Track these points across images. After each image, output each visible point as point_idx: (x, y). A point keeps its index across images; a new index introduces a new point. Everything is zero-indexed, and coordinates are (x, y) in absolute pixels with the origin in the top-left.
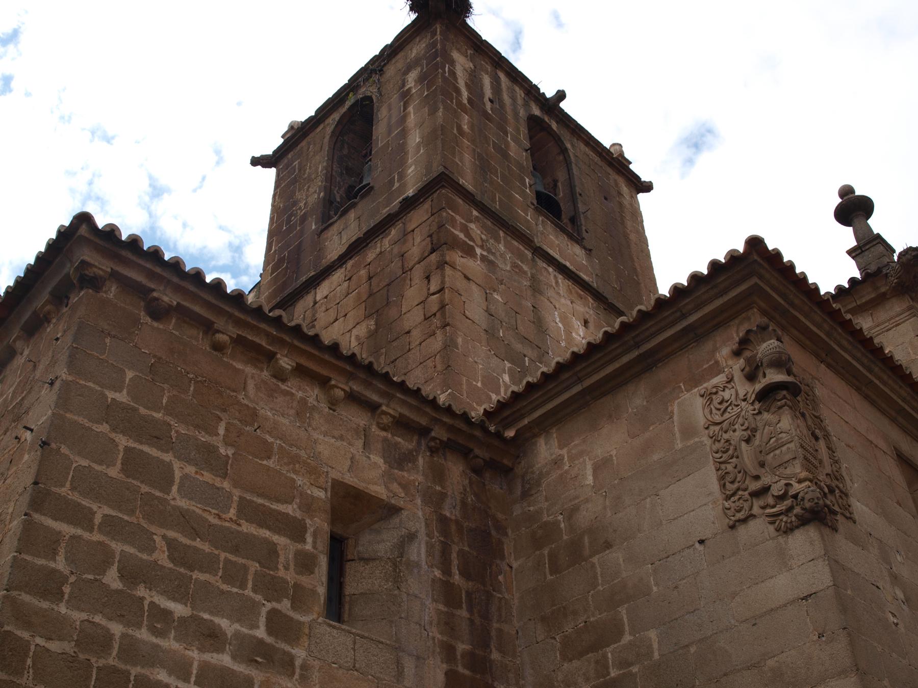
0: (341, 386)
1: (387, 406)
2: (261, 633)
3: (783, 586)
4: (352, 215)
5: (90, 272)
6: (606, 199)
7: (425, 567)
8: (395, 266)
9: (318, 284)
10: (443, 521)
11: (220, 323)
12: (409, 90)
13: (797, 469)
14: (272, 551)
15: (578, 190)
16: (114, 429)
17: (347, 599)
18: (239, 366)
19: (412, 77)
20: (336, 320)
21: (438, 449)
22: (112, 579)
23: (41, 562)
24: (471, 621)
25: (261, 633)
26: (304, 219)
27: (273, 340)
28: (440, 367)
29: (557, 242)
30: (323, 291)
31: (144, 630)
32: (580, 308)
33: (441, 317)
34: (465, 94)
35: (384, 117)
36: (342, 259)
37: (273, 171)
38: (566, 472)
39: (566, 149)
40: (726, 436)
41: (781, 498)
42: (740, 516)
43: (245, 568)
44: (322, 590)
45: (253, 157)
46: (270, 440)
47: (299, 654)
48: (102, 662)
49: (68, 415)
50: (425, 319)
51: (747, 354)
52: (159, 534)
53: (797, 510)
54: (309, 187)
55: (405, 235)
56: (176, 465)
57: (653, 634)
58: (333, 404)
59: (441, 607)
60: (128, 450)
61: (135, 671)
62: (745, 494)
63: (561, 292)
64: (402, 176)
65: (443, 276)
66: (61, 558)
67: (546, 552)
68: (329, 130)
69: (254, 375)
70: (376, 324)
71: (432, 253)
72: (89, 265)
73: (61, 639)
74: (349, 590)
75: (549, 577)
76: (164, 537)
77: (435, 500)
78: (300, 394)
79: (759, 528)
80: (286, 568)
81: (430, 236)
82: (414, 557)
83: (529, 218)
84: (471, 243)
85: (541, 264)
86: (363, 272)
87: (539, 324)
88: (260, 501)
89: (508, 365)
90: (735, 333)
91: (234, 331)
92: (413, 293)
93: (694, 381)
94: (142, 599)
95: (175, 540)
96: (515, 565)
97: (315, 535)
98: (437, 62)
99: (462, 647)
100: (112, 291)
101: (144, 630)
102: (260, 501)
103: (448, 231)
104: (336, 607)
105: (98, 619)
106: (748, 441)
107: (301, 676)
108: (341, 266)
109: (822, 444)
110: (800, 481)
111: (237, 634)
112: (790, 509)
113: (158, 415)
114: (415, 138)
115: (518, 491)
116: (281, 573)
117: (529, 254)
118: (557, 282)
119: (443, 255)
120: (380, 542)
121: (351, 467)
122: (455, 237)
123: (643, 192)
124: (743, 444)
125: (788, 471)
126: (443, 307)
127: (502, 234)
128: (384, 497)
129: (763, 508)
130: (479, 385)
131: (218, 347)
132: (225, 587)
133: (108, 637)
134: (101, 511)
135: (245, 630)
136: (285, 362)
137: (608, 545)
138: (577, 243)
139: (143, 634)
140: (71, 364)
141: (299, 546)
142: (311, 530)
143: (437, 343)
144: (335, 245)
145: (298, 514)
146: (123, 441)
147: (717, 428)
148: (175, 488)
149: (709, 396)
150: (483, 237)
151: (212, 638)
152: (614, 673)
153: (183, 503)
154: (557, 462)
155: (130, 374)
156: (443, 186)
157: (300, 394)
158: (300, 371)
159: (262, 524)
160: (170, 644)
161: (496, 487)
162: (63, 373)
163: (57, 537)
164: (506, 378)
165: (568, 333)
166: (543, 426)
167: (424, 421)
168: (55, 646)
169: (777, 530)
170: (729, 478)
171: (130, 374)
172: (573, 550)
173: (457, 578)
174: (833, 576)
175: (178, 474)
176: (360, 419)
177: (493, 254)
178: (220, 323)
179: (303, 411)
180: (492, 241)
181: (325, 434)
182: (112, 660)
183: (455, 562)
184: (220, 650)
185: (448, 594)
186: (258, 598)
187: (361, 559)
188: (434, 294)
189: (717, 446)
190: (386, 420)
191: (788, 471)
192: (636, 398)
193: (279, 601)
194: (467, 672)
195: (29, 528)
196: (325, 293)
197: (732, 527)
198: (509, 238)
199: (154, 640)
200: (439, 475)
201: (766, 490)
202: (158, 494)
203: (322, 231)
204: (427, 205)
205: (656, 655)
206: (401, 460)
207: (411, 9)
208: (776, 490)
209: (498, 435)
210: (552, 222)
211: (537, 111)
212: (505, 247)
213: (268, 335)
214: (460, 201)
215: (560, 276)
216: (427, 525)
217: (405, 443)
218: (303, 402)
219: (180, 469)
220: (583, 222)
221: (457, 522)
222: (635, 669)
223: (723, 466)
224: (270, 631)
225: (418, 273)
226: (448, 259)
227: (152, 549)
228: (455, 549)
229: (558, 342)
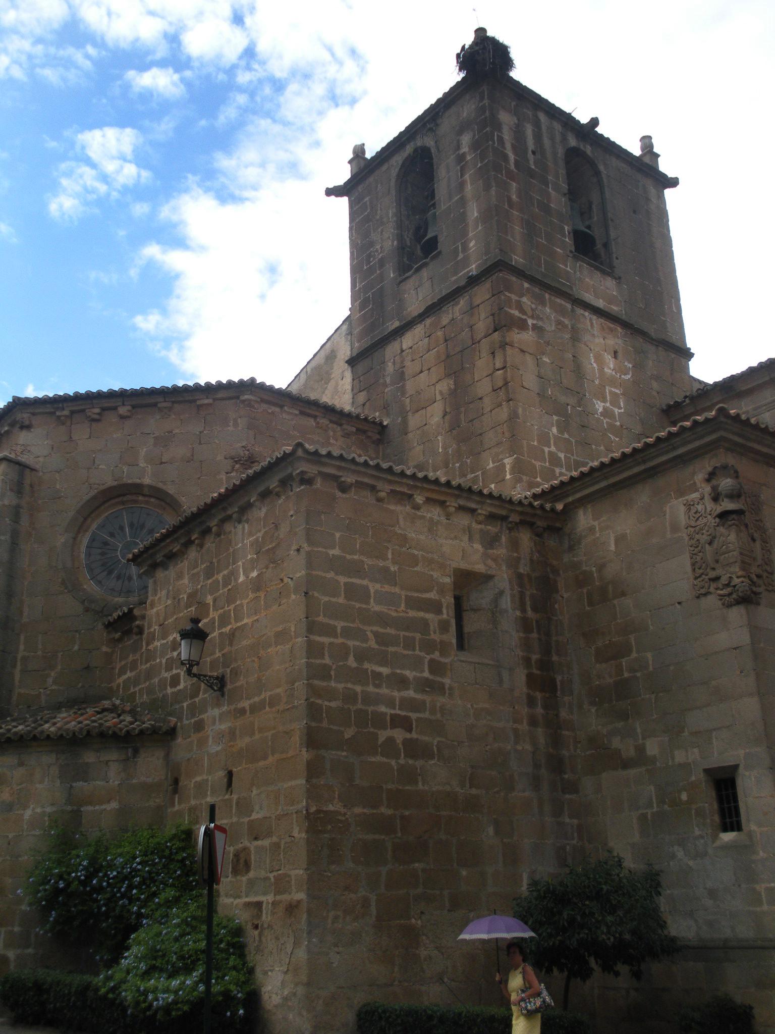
0: (453, 503)
1: (481, 509)
2: (426, 674)
3: (723, 639)
4: (425, 273)
5: (306, 477)
6: (634, 212)
7: (510, 611)
8: (466, 334)
9: (403, 334)
10: (520, 576)
11: (380, 485)
12: (464, 155)
13: (736, 569)
14: (425, 624)
15: (610, 215)
16: (336, 574)
17: (466, 635)
18: (392, 507)
19: (466, 140)
20: (421, 372)
21: (514, 527)
22: (352, 662)
23: (318, 661)
24: (540, 639)
25: (426, 674)
26: (382, 263)
27: (410, 487)
28: (507, 434)
29: (592, 283)
30: (407, 341)
31: (371, 686)
32: (611, 342)
33: (505, 390)
34: (512, 157)
35: (445, 174)
36: (422, 317)
37: (345, 200)
38: (598, 538)
39: (600, 172)
40: (697, 537)
41: (728, 585)
42: (703, 591)
43: (414, 638)
44: (454, 641)
45: (327, 189)
46: (416, 552)
47: (447, 681)
48: (355, 708)
49: (314, 573)
50: (494, 390)
51: (714, 482)
52: (369, 630)
53: (734, 596)
54: (382, 231)
55: (472, 308)
56: (371, 585)
57: (649, 655)
58: (448, 516)
59: (522, 635)
60: (345, 584)
61: (370, 709)
62: (706, 577)
63: (596, 333)
64: (465, 248)
65: (505, 356)
66: (327, 657)
67: (585, 591)
68: (394, 172)
69: (401, 510)
70: (455, 385)
71: (495, 331)
72: (306, 472)
73: (335, 700)
74: (467, 630)
75: (588, 608)
76: (372, 631)
77: (513, 563)
78: (429, 515)
79: (712, 601)
80: (435, 633)
81: (493, 315)
82: (504, 606)
83: (568, 269)
84: (524, 317)
85: (579, 311)
86: (440, 334)
87: (578, 370)
88: (416, 595)
89: (555, 418)
90: (707, 465)
91: (388, 488)
92: (482, 364)
93: (681, 493)
94: (367, 669)
95: (377, 632)
96: (565, 596)
97: (447, 608)
98: (487, 125)
99: (535, 657)
100: (319, 484)
101: (371, 686)
102: (416, 595)
103: (507, 313)
104: (461, 646)
105: (350, 685)
106: (710, 543)
107: (450, 694)
108: (420, 322)
109: (758, 544)
110: (738, 577)
111: (415, 678)
112: (730, 594)
113: (356, 557)
114: (474, 212)
115: (566, 546)
116: (433, 636)
117: (569, 306)
118: (592, 324)
119: (504, 337)
120: (482, 598)
121: (463, 556)
122: (512, 316)
123: (669, 187)
124: (707, 546)
125: (732, 569)
126: (506, 384)
127: (547, 296)
128: (483, 571)
129: (716, 589)
130: (535, 443)
131: (379, 500)
132: (406, 652)
133: (356, 694)
134: (339, 625)
135: (418, 675)
136: (419, 499)
137: (623, 594)
138: (609, 274)
139: (371, 689)
140: (309, 540)
141: (440, 617)
142: (445, 605)
143: (503, 413)
144: (415, 304)
145: (437, 598)
146: (342, 579)
147: (692, 530)
148: (372, 601)
149: (689, 506)
150: (533, 306)
151: (403, 683)
152: (626, 675)
153: (377, 608)
154: (592, 530)
155: (338, 535)
156: (500, 271)
157: (429, 515)
158: (428, 500)
159: (420, 609)
160: (384, 691)
161: (551, 542)
162: (306, 547)
163: (322, 645)
164: (555, 430)
165: (601, 370)
166: (582, 502)
167: (504, 513)
168: (333, 704)
169: (723, 604)
170: (697, 566)
171: (338, 535)
172: (602, 592)
173: (530, 613)
174: (751, 636)
175: (372, 591)
176: (464, 520)
177: (541, 319)
178: (380, 485)
179: (432, 526)
180: (540, 307)
181: (446, 538)
182: (360, 706)
183: (528, 603)
184: (407, 689)
185: (525, 625)
186: (422, 654)
187: (472, 610)
188: (498, 370)
189: (693, 542)
190: (481, 518)
191: (732, 569)
192: (643, 495)
193: (433, 653)
194: (538, 672)
195: (310, 645)
196: (410, 344)
197: (698, 597)
198: (553, 298)
199: (377, 690)
200: (515, 545)
201: (717, 579)
202: (364, 606)
203: (401, 282)
204: (487, 285)
205: (651, 669)
206: (490, 542)
207: (460, 70)
208: (724, 580)
209: (553, 510)
210: (588, 264)
211: (573, 142)
212: (551, 308)
213: (408, 485)
214: (514, 279)
215: (595, 317)
216: (510, 582)
217: (492, 529)
218: (431, 520)
219: (373, 587)
220: (614, 250)
221: (528, 575)
222: (638, 674)
223: (694, 557)
224: (431, 672)
225: (485, 345)
226: (508, 340)
227: (366, 640)
228: (528, 593)
229: (593, 381)
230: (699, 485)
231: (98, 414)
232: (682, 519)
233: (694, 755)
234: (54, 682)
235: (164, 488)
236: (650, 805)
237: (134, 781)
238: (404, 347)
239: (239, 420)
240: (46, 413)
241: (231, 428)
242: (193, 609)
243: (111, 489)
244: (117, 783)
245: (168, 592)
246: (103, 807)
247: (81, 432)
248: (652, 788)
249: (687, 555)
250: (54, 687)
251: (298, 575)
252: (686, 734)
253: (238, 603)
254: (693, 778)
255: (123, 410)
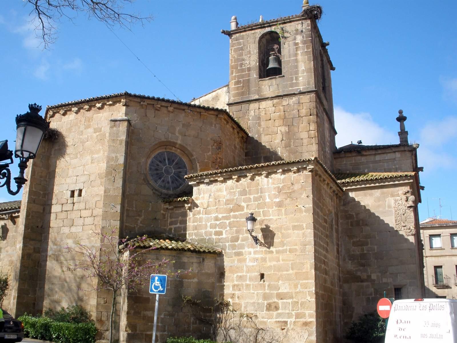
12: (298, 43)
57: (376, 247)
64: (297, 79)
75: (350, 227)
137: (367, 225)
149: (396, 201)
152: (365, 252)
205: (376, 251)
222: (370, 252)
230: (400, 195)
231: (159, 108)
232: (393, 205)
233: (390, 280)
234: (141, 223)
235: (186, 147)
236: (371, 294)
237: (203, 271)
238: (261, 107)
239: (217, 125)
240: (137, 102)
241: (213, 127)
242: (231, 206)
243: (163, 142)
244: (197, 271)
245: (210, 195)
246: (192, 280)
247: (151, 113)
248: (373, 289)
249: (394, 217)
250: (141, 225)
251: (307, 206)
252: (388, 273)
253: (265, 209)
254: (389, 287)
255: (171, 109)
